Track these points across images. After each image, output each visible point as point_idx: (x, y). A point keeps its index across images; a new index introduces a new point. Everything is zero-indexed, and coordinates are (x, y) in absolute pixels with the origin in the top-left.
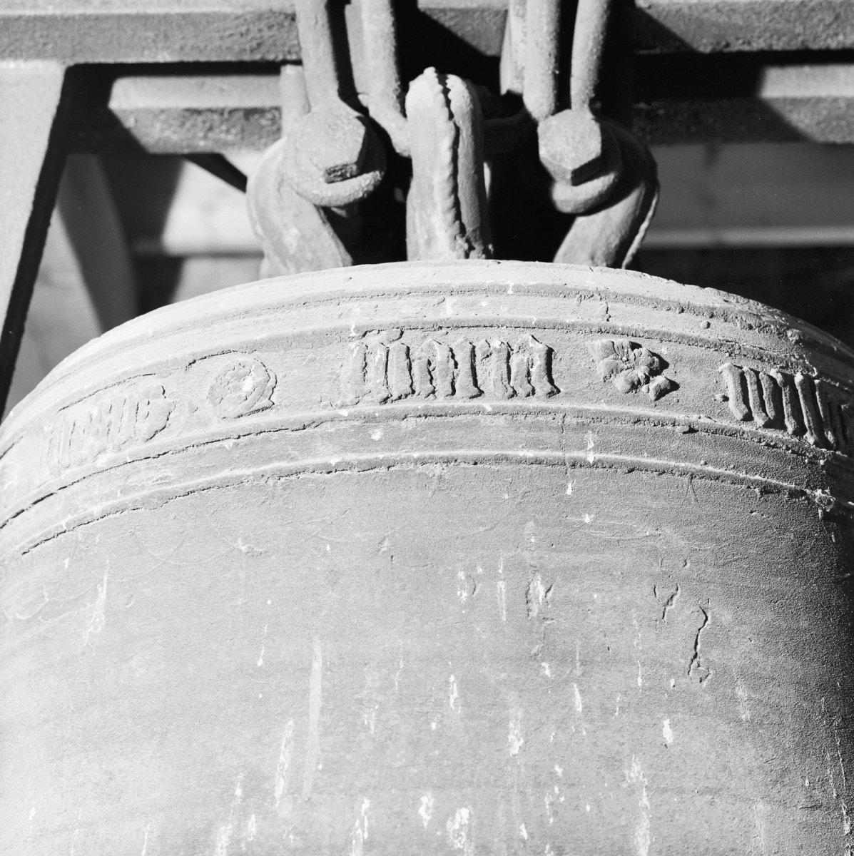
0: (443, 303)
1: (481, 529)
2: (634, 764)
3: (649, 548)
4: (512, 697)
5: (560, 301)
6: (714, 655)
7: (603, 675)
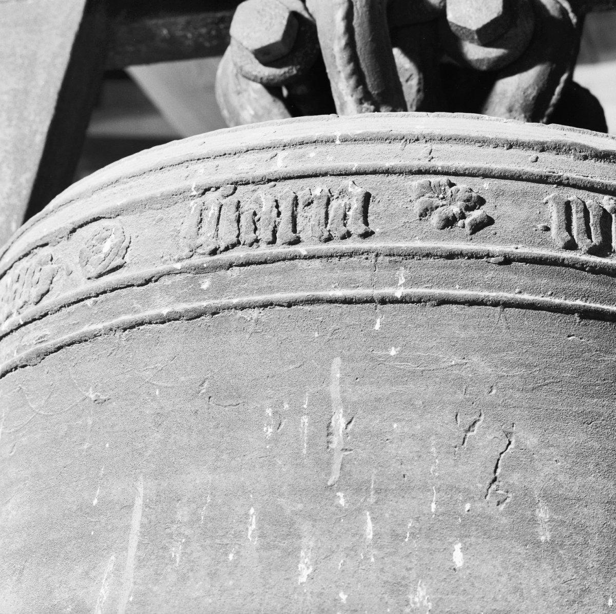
0: (276, 157)
1: (291, 367)
2: (419, 589)
3: (452, 377)
5: (384, 146)
6: (515, 478)
7: (397, 502)
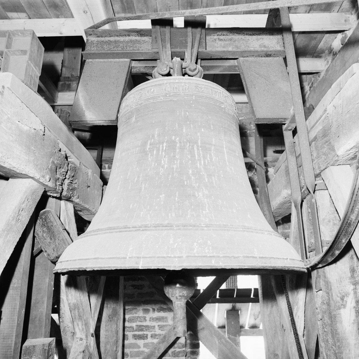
4: (184, 125)
